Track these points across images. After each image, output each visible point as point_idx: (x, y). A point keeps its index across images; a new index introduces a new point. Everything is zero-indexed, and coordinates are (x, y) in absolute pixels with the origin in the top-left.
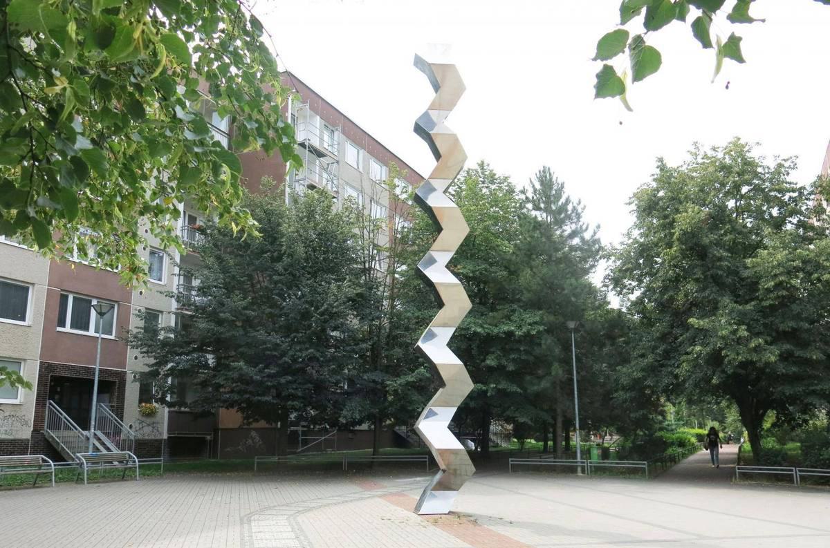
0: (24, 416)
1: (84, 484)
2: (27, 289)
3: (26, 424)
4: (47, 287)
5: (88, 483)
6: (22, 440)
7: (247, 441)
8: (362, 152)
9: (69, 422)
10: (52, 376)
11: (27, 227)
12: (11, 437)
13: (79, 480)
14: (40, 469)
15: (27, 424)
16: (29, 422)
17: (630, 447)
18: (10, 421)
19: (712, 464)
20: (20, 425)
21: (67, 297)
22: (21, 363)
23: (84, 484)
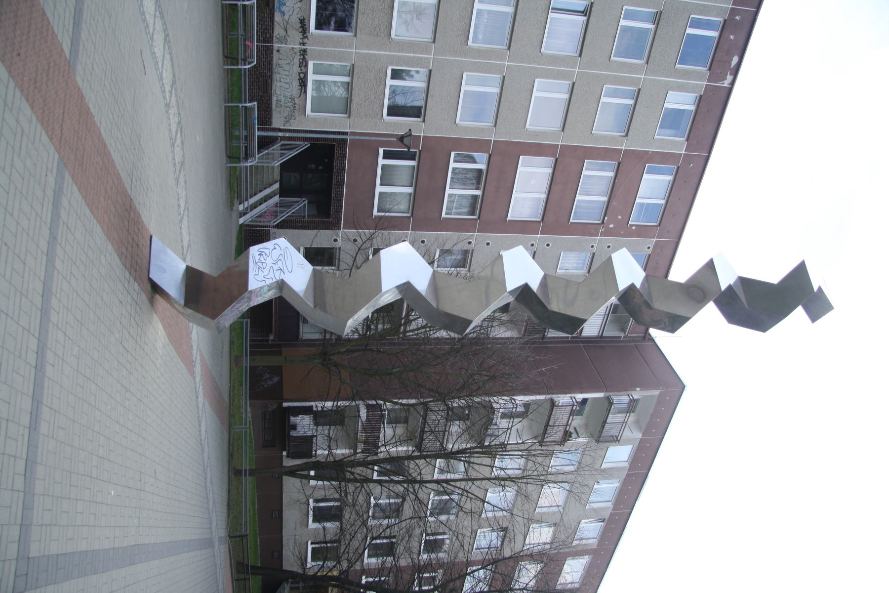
0: (295, 119)
1: (225, 103)
2: (419, 117)
3: (288, 120)
4: (422, 135)
5: (225, 107)
6: (270, 118)
7: (268, 374)
8: (610, 505)
9: (289, 155)
10: (334, 145)
11: (366, 582)
12: (274, 106)
13: (232, 156)
14: (242, 60)
15: (287, 122)
16: (288, 124)
17: (406, 288)
18: (290, 104)
19: (318, 405)
20: (285, 115)
21: (413, 159)
22: (346, 114)
23: (225, 103)
